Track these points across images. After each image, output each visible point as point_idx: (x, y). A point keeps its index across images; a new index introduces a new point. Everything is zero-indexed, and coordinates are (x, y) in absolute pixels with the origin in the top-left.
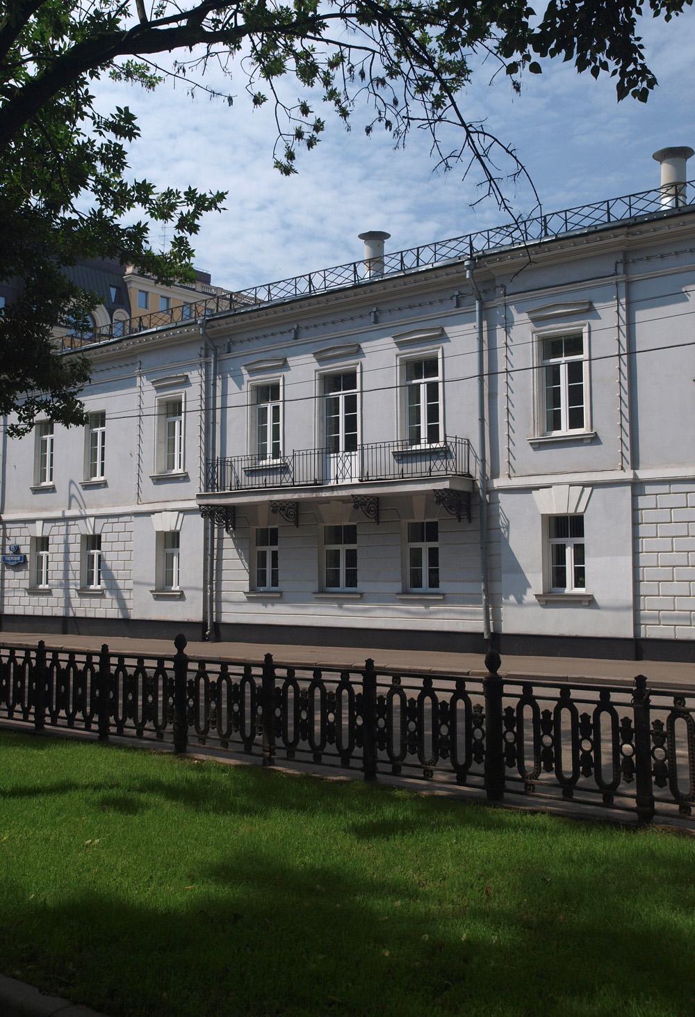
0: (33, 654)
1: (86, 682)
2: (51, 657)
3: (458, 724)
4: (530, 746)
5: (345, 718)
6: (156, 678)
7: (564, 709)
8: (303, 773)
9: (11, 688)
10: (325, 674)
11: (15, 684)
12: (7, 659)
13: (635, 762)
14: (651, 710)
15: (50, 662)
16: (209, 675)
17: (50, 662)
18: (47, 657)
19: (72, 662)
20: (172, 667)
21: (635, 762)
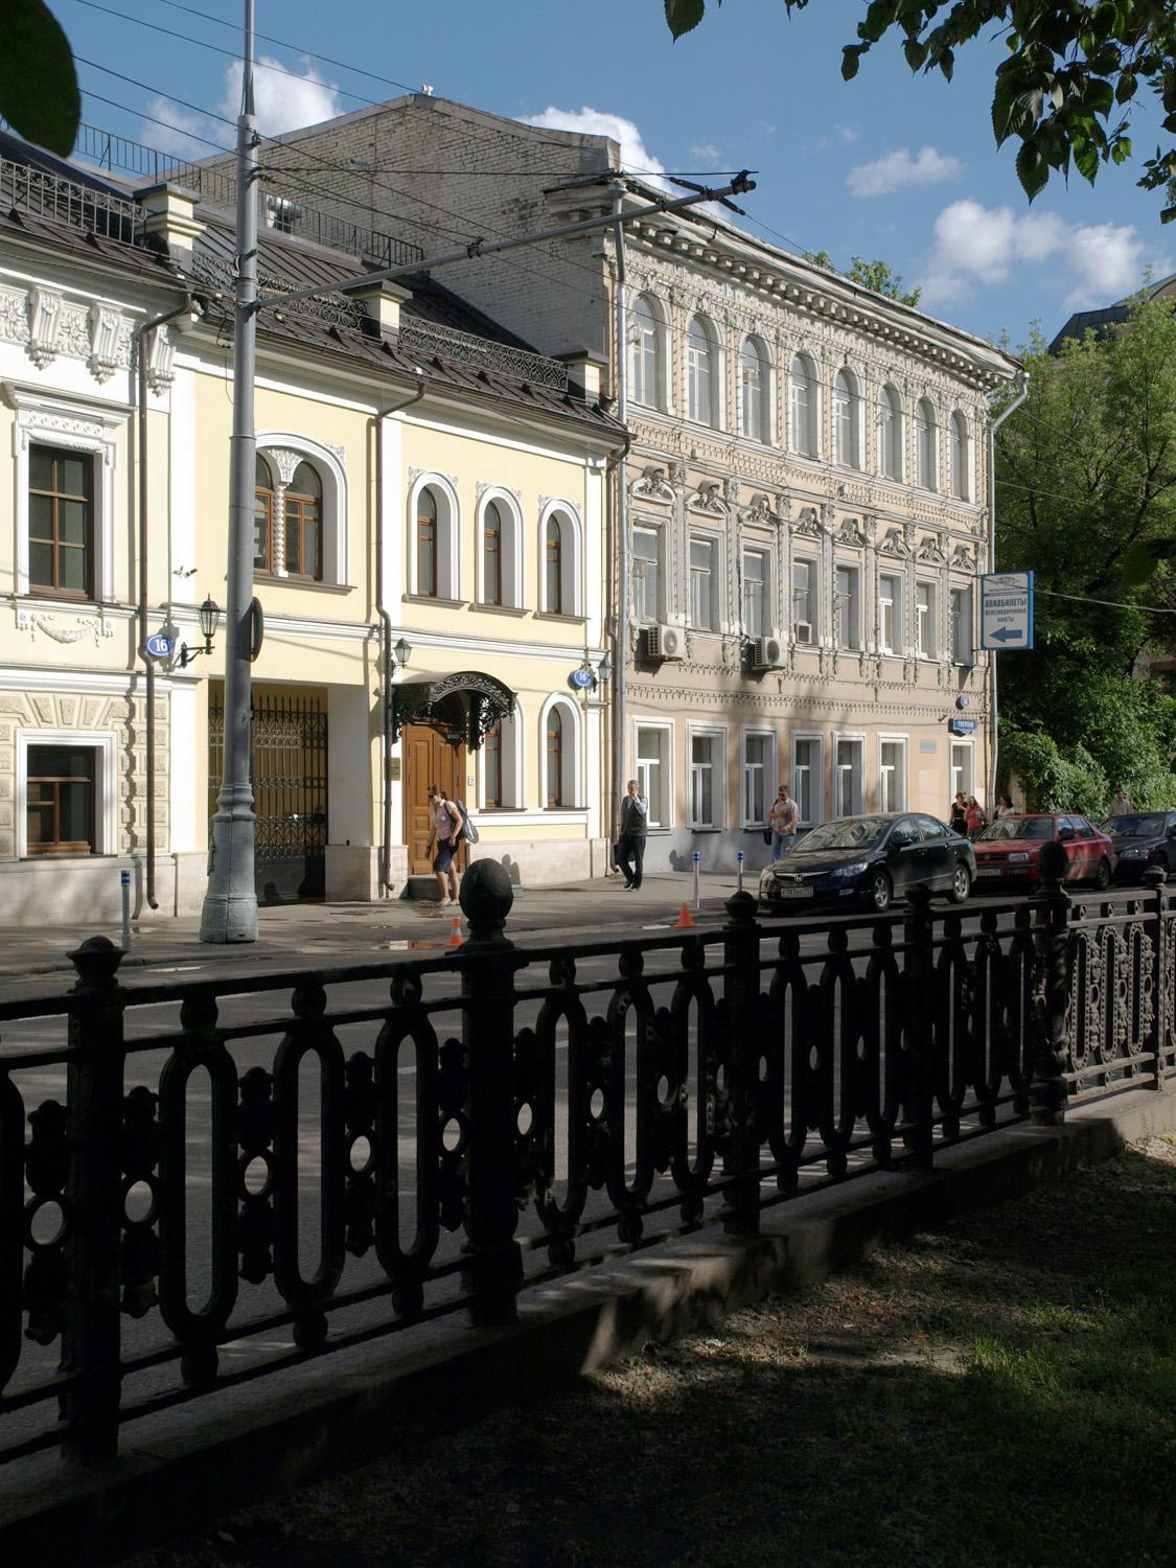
0: (715, 954)
1: (833, 1029)
2: (775, 955)
3: (415, 1125)
4: (409, 1197)
5: (309, 1122)
6: (617, 1020)
7: (202, 1066)
8: (1097, 1356)
9: (631, 1076)
10: (285, 1007)
11: (872, 1048)
12: (673, 985)
13: (26, 1182)
14: (848, 932)
15: (1011, 939)
16: (232, 1046)
17: (1011, 939)
18: (965, 932)
19: (632, 985)
20: (998, 916)
21: (26, 1182)
